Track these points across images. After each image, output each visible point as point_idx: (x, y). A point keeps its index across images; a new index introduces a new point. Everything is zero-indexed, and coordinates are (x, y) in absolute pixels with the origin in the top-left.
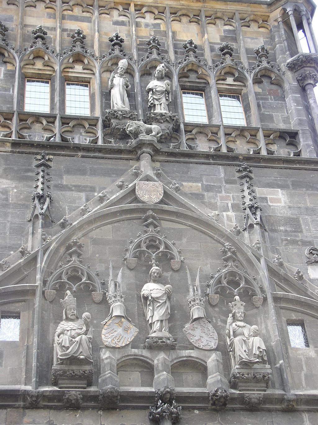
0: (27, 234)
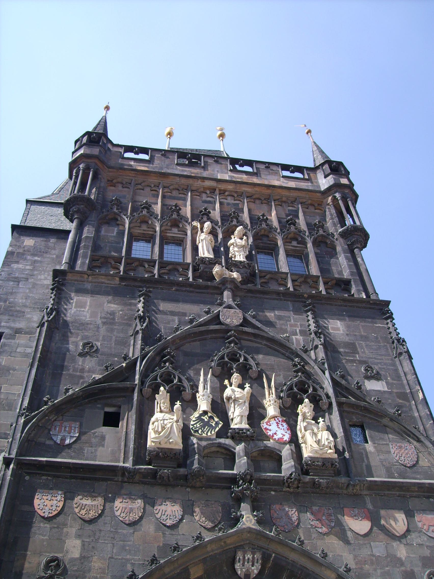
0: (129, 346)
